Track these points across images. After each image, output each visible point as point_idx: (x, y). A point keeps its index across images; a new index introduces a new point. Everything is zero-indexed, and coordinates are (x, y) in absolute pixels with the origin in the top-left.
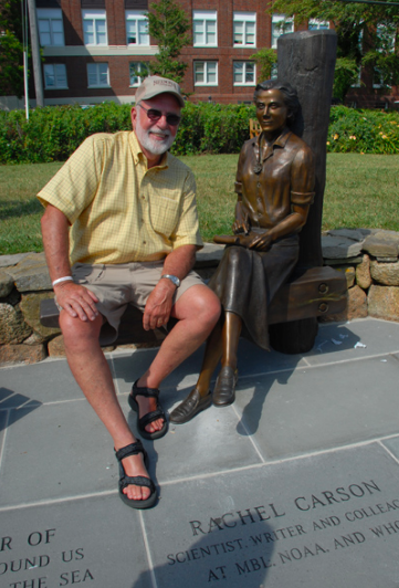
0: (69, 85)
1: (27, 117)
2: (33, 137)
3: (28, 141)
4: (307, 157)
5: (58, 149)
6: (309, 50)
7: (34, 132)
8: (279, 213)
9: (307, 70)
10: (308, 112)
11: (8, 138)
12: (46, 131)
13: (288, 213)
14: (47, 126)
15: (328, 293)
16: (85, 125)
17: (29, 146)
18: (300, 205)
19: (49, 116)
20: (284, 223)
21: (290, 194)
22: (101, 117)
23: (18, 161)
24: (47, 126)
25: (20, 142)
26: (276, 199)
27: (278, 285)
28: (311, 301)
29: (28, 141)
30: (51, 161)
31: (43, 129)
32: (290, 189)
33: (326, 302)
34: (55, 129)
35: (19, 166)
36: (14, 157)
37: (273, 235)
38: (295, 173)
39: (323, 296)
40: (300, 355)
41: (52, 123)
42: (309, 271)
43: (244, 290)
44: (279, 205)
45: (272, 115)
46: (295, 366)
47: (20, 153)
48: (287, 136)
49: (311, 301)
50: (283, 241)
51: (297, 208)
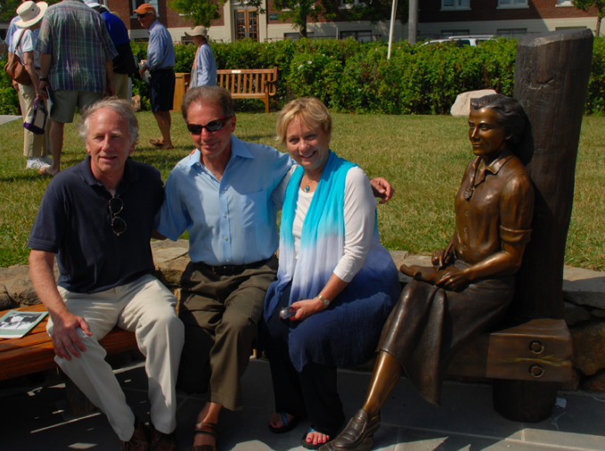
0: (471, 6)
1: (389, 57)
2: (389, 83)
3: (383, 86)
4: (520, 187)
5: (418, 98)
6: (542, 60)
7: (393, 76)
8: (487, 247)
9: (539, 83)
10: (539, 132)
11: (361, 82)
12: (406, 75)
13: (497, 249)
14: (409, 70)
15: (544, 354)
16: (455, 70)
17: (384, 93)
18: (509, 243)
19: (412, 57)
20: (487, 262)
21: (499, 231)
22: (477, 60)
23: (369, 109)
24: (409, 70)
25: (373, 87)
26: (482, 232)
27: (467, 333)
28: (519, 359)
29: (383, 86)
30: (407, 113)
31: (403, 73)
32: (499, 223)
33: (539, 365)
34: (417, 74)
35: (366, 116)
36: (365, 104)
37: (470, 273)
38: (503, 206)
39: (536, 357)
40: (522, 424)
41: (415, 66)
42: (533, 322)
43: (409, 331)
44: (485, 239)
45: (481, 137)
46: (507, 436)
47: (373, 100)
48: (504, 160)
49: (519, 359)
50: (484, 282)
51: (506, 245)
